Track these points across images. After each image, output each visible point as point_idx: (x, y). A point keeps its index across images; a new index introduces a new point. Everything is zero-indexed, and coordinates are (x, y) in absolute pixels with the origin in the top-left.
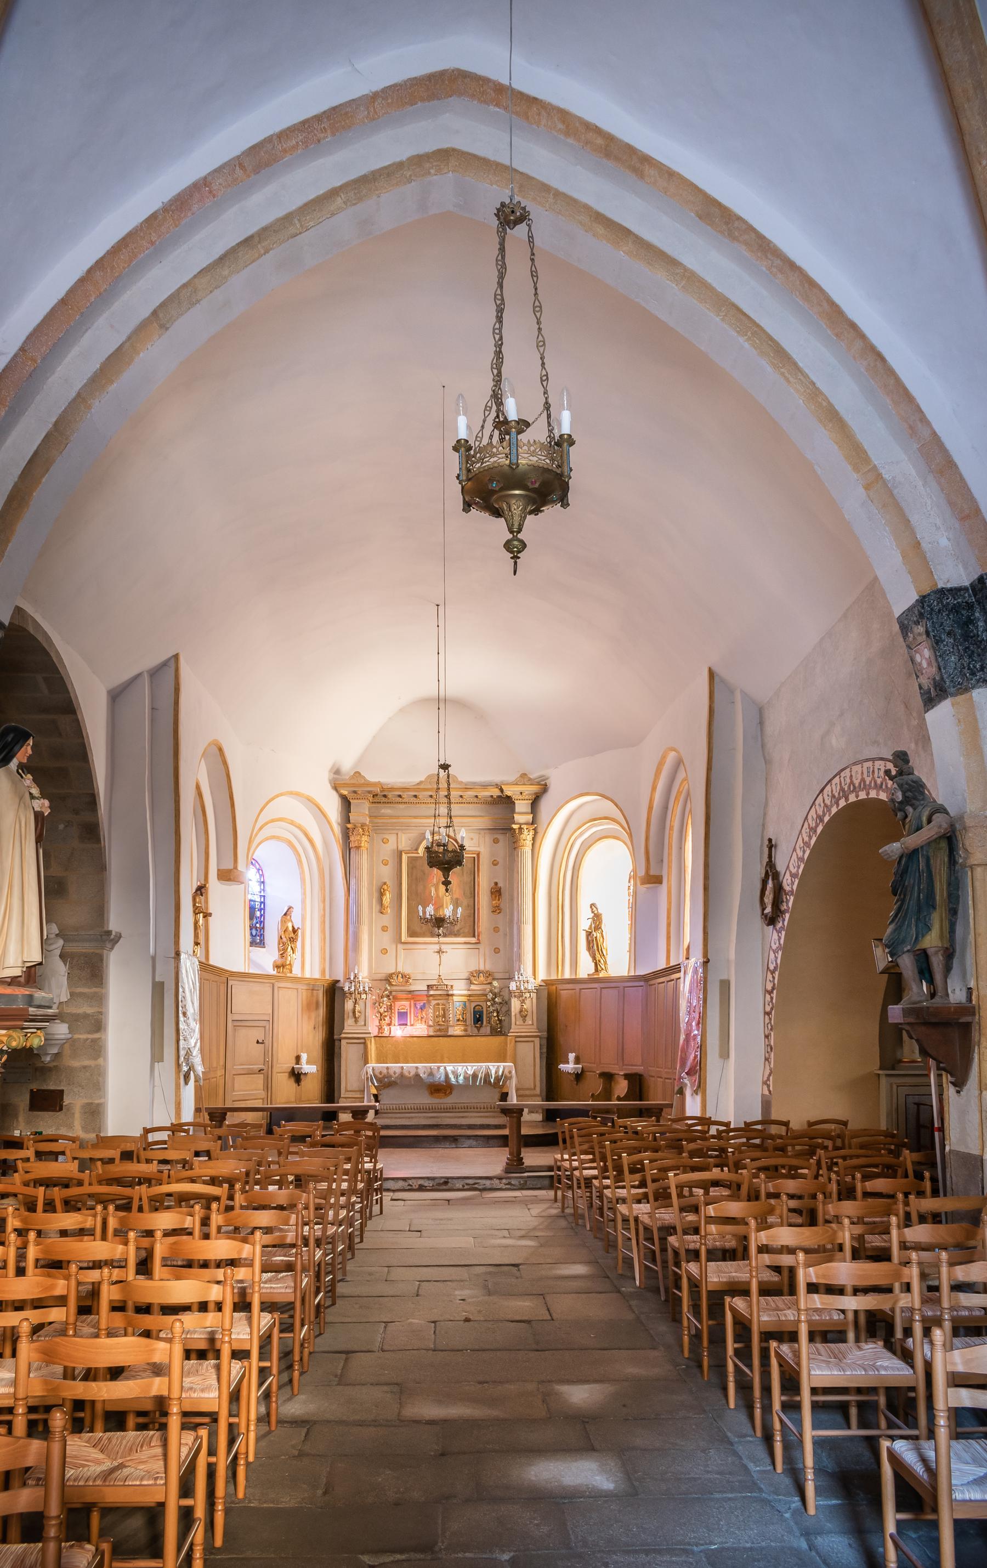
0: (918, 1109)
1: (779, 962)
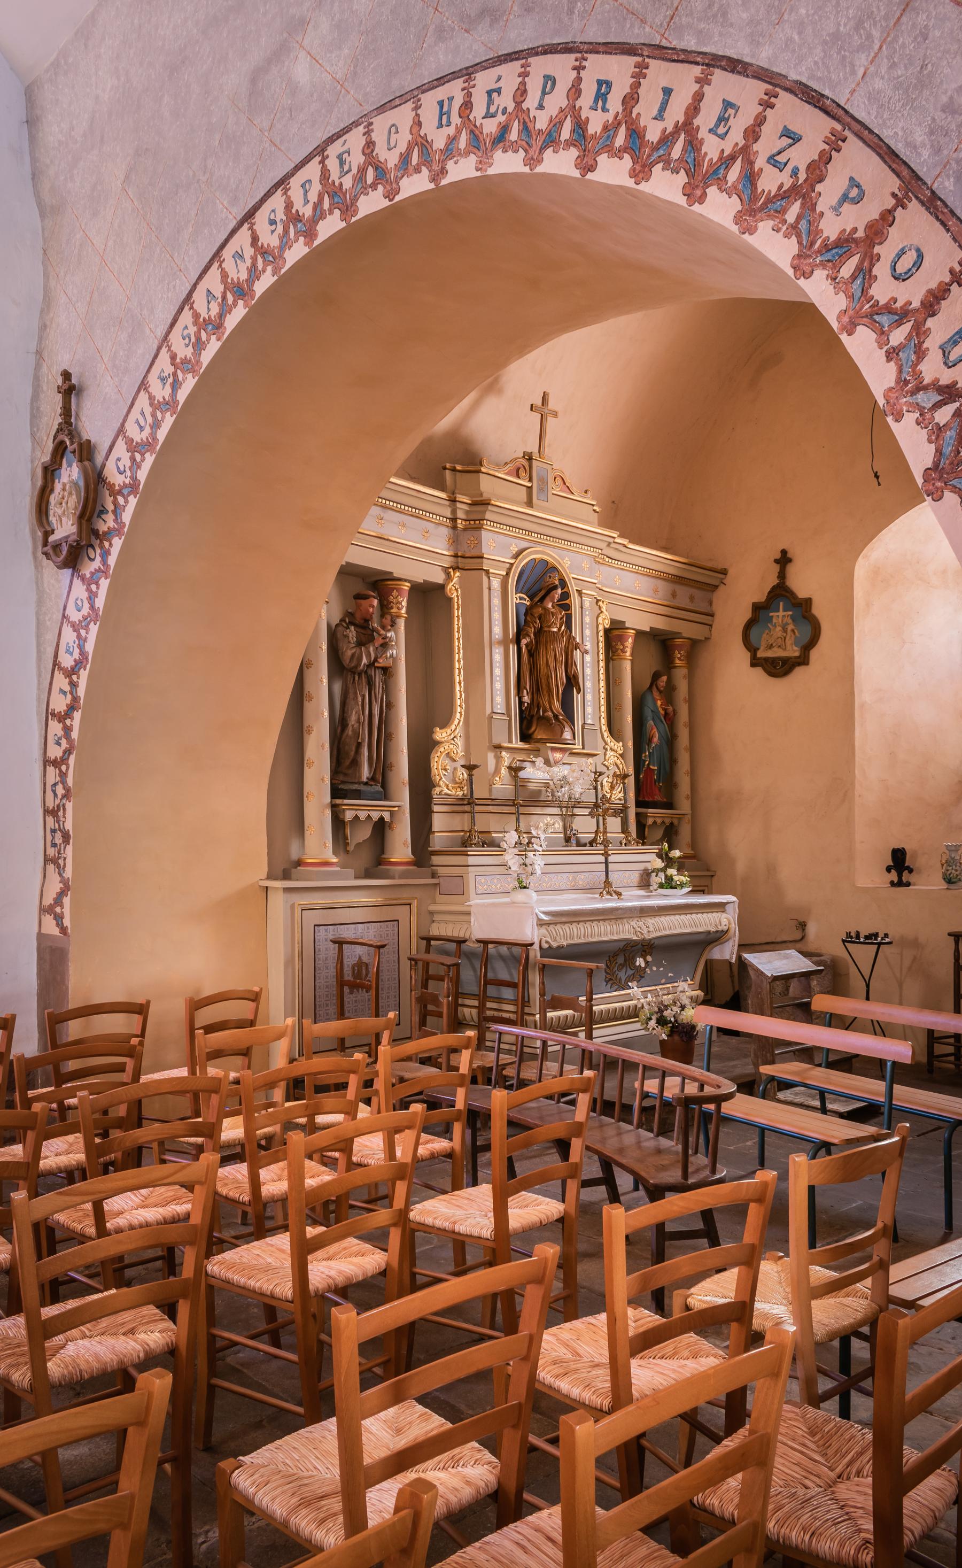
0: (341, 951)
1: (90, 647)
